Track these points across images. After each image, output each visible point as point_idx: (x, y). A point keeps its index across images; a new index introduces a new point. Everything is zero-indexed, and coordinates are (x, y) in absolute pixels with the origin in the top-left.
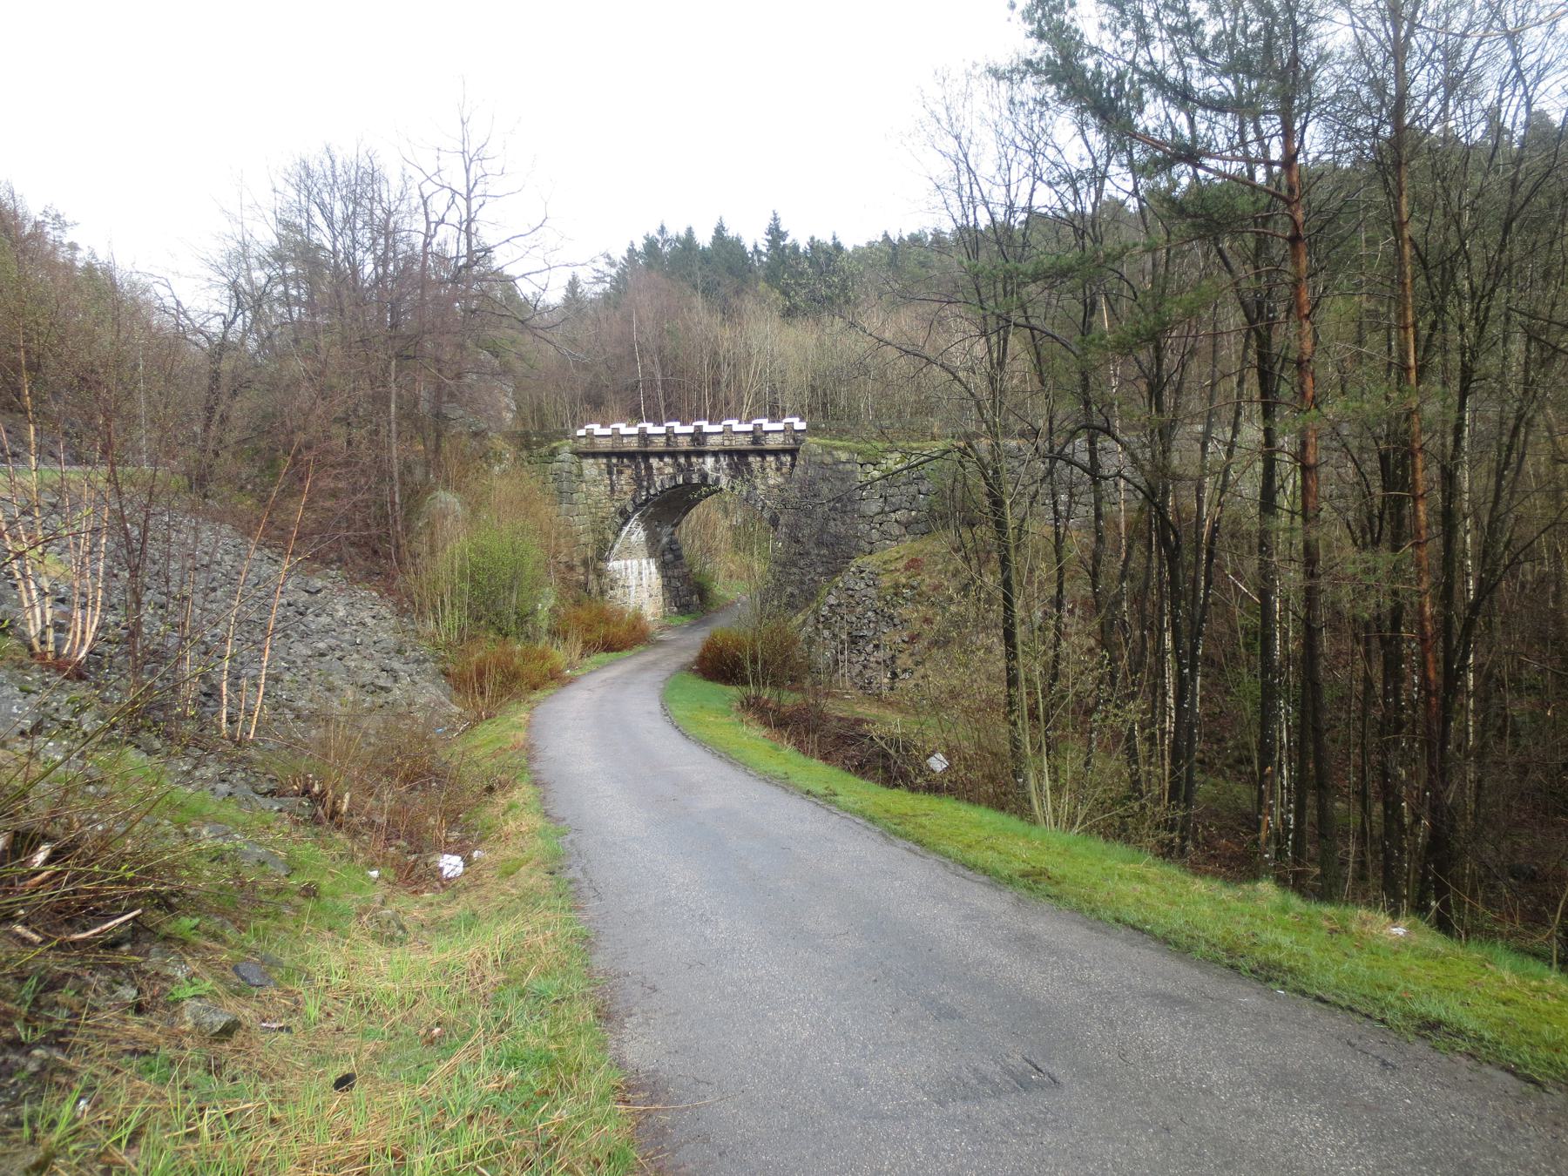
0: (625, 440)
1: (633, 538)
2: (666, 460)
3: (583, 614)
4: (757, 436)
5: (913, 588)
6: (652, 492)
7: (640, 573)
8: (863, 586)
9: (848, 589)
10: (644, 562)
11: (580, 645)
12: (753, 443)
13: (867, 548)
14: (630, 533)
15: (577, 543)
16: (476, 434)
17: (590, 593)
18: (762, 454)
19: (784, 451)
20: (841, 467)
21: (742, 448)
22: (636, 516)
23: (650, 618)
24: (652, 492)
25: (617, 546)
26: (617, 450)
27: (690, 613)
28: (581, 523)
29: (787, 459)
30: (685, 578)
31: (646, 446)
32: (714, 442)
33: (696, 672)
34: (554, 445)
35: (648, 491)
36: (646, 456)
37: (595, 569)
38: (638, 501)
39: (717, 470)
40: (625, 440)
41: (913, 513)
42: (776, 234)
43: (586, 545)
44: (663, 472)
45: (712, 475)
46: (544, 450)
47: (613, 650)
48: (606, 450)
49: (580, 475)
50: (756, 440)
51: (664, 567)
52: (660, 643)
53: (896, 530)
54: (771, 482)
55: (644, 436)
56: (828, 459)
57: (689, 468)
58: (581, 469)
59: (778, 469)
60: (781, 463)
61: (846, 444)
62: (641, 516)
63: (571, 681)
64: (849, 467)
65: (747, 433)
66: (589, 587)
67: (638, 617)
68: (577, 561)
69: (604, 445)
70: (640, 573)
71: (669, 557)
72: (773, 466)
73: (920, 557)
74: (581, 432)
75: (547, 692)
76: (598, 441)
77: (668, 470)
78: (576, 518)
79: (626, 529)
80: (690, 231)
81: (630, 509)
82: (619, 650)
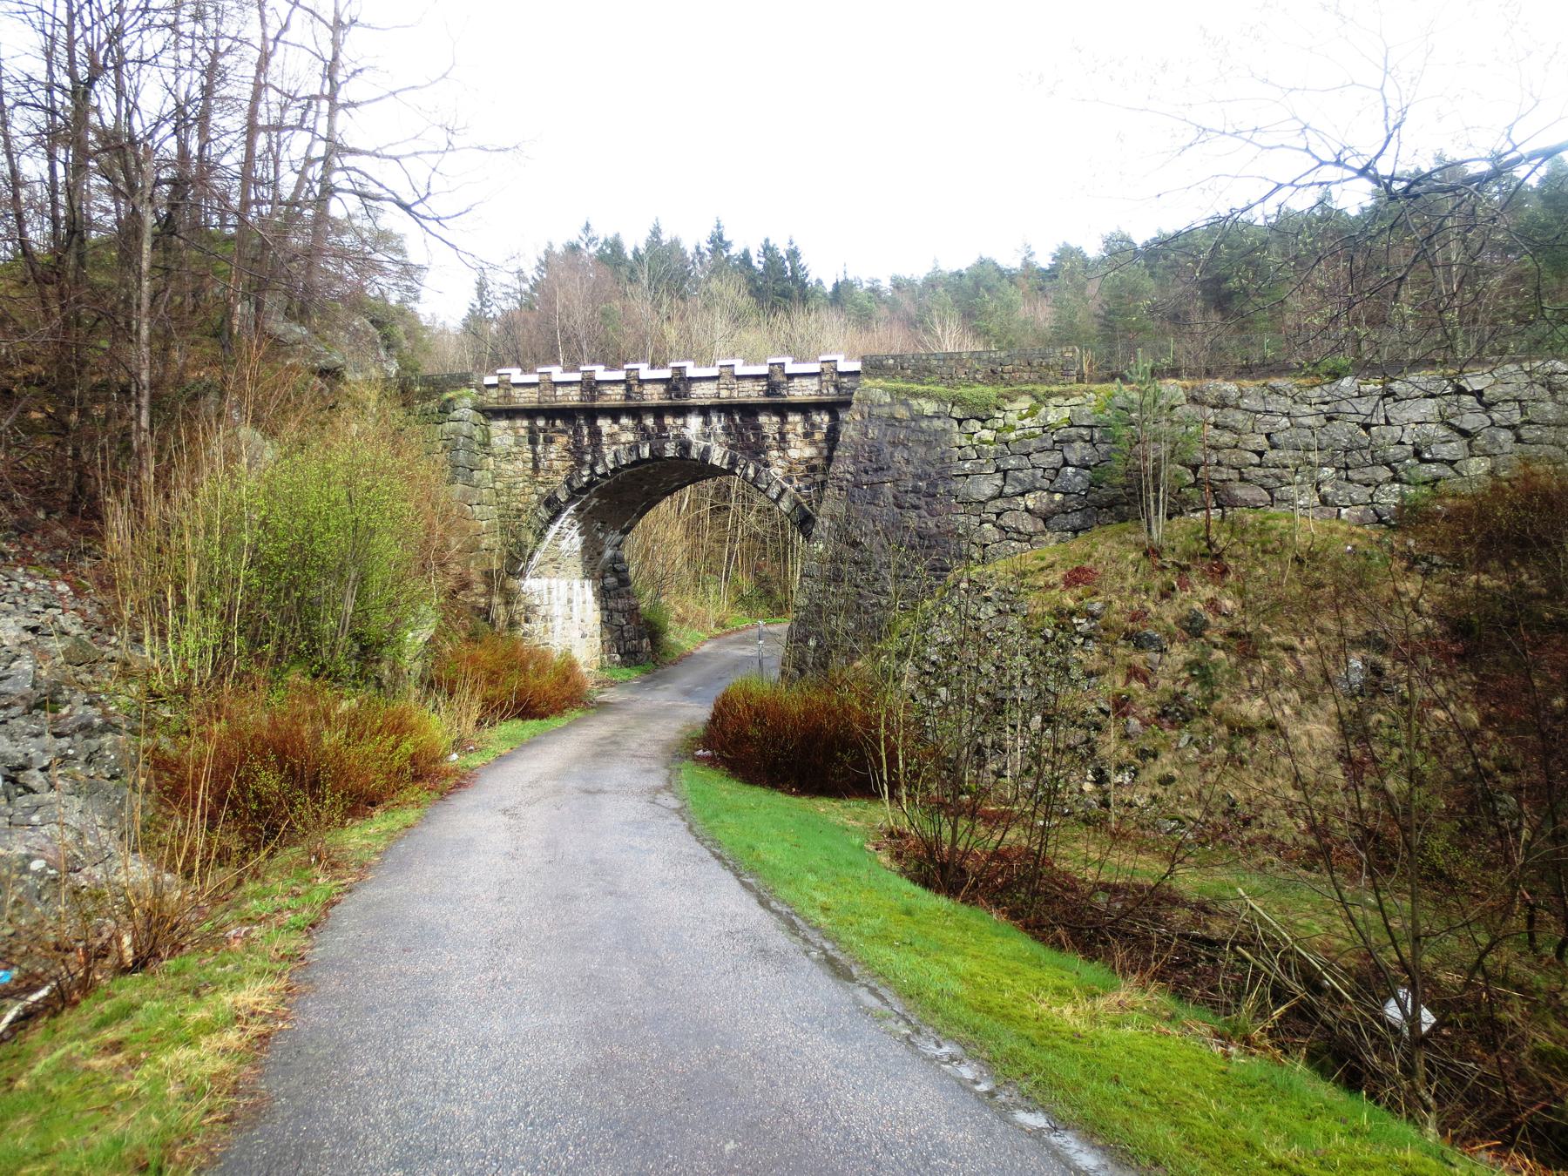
1: (564, 545)
3: (483, 654)
5: (1092, 616)
6: (599, 470)
7: (570, 601)
10: (577, 584)
12: (767, 394)
14: (559, 536)
15: (474, 548)
16: (323, 373)
17: (493, 624)
18: (781, 410)
19: (819, 406)
20: (924, 424)
21: (750, 400)
22: (571, 509)
23: (585, 670)
25: (538, 556)
26: (545, 405)
27: (637, 664)
28: (485, 517)
29: (823, 419)
30: (633, 612)
31: (593, 399)
32: (702, 393)
33: (712, 762)
34: (448, 395)
35: (592, 467)
36: (592, 414)
37: (502, 588)
38: (576, 485)
39: (707, 437)
40: (560, 391)
41: (1058, 497)
42: (718, 243)
43: (490, 550)
46: (432, 405)
48: (529, 405)
49: (486, 444)
50: (773, 389)
51: (604, 594)
52: (603, 707)
53: (1028, 524)
54: (794, 453)
55: (591, 386)
56: (901, 412)
58: (488, 435)
59: (807, 435)
60: (813, 425)
61: (932, 388)
62: (579, 510)
63: (462, 781)
64: (938, 424)
65: (757, 377)
66: (493, 615)
67: (572, 665)
68: (475, 575)
69: (525, 398)
70: (570, 601)
71: (611, 580)
72: (800, 430)
73: (1088, 564)
78: (477, 509)
79: (554, 528)
82: (542, 716)
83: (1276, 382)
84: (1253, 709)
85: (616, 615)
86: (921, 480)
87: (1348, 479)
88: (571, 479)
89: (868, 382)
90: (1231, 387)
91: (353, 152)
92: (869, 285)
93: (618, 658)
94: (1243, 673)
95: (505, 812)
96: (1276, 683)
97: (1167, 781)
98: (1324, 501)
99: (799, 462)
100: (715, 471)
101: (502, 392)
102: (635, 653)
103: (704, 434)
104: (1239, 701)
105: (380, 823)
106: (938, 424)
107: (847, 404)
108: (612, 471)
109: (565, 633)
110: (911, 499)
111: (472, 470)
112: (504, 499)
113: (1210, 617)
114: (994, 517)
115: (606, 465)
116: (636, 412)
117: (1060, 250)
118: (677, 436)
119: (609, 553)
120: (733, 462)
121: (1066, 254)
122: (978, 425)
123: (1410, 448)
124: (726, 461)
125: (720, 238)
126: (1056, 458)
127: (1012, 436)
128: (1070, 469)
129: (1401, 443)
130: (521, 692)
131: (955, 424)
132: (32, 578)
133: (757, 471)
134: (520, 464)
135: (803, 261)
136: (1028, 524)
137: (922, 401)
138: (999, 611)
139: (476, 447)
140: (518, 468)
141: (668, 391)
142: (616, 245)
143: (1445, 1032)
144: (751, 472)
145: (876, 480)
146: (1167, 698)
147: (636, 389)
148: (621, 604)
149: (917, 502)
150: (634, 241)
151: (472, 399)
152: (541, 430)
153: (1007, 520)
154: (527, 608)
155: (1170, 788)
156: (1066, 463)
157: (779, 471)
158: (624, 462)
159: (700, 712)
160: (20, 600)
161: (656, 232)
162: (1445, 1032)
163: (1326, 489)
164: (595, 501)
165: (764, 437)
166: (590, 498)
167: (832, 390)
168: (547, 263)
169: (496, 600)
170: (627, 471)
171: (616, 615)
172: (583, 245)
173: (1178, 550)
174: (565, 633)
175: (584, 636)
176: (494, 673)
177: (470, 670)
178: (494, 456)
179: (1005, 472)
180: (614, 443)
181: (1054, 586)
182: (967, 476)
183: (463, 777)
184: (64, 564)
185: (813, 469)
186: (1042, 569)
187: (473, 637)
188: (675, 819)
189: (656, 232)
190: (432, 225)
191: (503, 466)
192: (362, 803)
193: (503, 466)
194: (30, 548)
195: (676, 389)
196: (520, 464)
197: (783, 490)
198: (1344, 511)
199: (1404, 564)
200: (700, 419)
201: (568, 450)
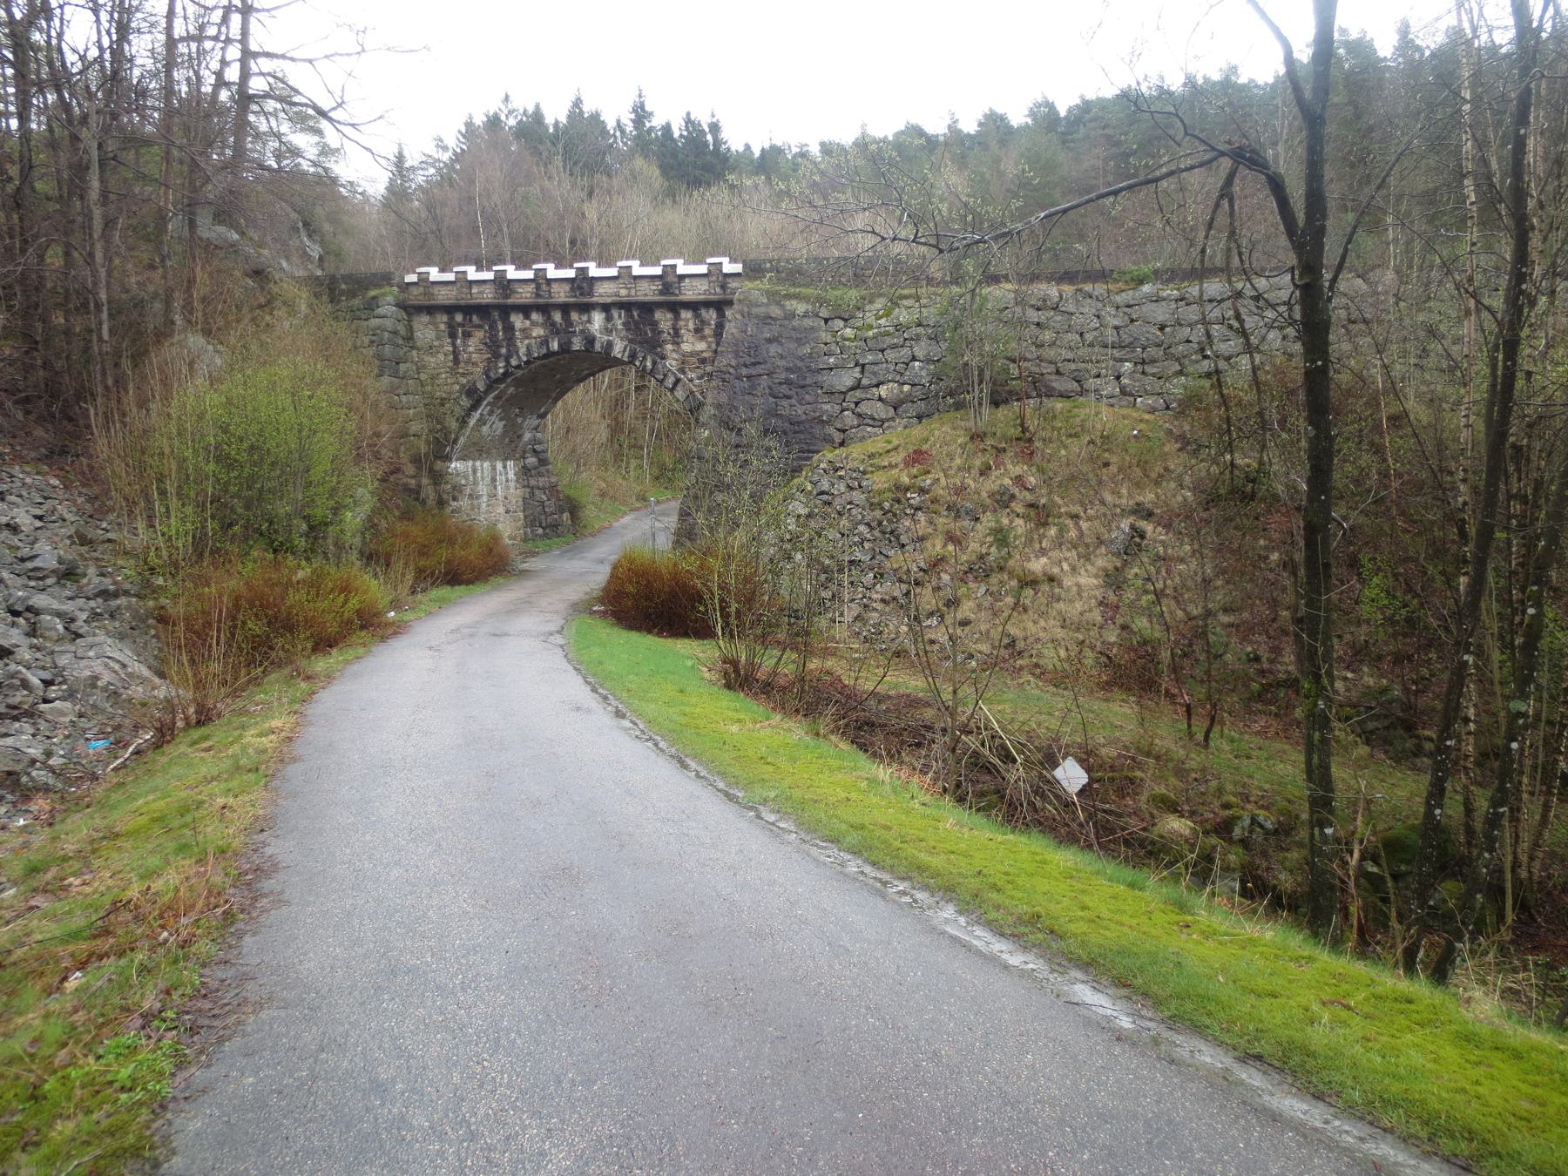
0: (475, 290)
1: (485, 429)
2: (535, 316)
3: (414, 530)
4: (669, 281)
5: (922, 491)
6: (514, 362)
7: (494, 480)
8: (843, 489)
9: (822, 493)
11: (410, 577)
12: (661, 293)
13: (838, 437)
17: (424, 502)
18: (675, 307)
19: (707, 304)
21: (647, 299)
22: (490, 398)
23: (508, 541)
24: (514, 362)
25: (462, 440)
26: (462, 302)
29: (711, 315)
30: (553, 489)
31: (507, 297)
32: (603, 292)
33: (603, 614)
34: (372, 293)
36: (506, 310)
37: (431, 470)
41: (906, 388)
42: (641, 114)
44: (530, 335)
45: (601, 339)
46: (356, 302)
47: (460, 583)
49: (409, 338)
54: (686, 347)
55: (502, 283)
56: (775, 311)
57: (565, 331)
58: (411, 329)
59: (697, 330)
60: (703, 322)
61: (804, 290)
62: (498, 398)
63: (398, 629)
66: (423, 495)
67: (495, 538)
69: (444, 296)
71: (531, 460)
72: (691, 326)
73: (925, 447)
74: (411, 278)
75: (350, 654)
76: (436, 290)
77: (538, 332)
78: (404, 399)
79: (476, 415)
80: (537, 106)
81: (481, 386)
82: (469, 582)
83: (1088, 287)
84: (1037, 565)
85: (537, 492)
86: (793, 373)
87: (1143, 373)
88: (489, 370)
89: (749, 285)
90: (1053, 291)
91: (268, 55)
92: (798, 150)
93: (540, 531)
94: (1036, 537)
95: (430, 648)
96: (1060, 545)
97: (965, 623)
98: (1123, 392)
99: (692, 354)
100: (617, 362)
101: (421, 289)
102: (556, 526)
103: (606, 329)
104: (1029, 560)
105: (336, 657)
106: (808, 322)
107: (730, 303)
108: (525, 363)
109: (490, 509)
110: (784, 389)
111: (398, 363)
112: (429, 388)
113: (1016, 491)
114: (853, 406)
115: (519, 357)
116: (545, 309)
117: (985, 116)
118: (582, 331)
119: (527, 436)
120: (633, 356)
121: (995, 123)
122: (841, 323)
123: (1196, 346)
124: (627, 354)
125: (642, 106)
126: (905, 352)
127: (870, 333)
128: (917, 363)
129: (1188, 341)
130: (448, 562)
131: (823, 323)
132: (28, 473)
133: (654, 363)
134: (441, 357)
135: (724, 135)
136: (881, 411)
137: (794, 302)
138: (848, 486)
139: (400, 342)
140: (441, 359)
141: (572, 289)
142: (537, 116)
143: (1096, 786)
144: (649, 364)
145: (754, 373)
146: (974, 557)
147: (544, 287)
148: (542, 481)
149: (790, 393)
150: (556, 114)
151: (395, 296)
152: (459, 325)
153: (864, 408)
154: (454, 488)
155: (967, 629)
156: (914, 359)
157: (674, 363)
158: (536, 355)
159: (599, 577)
160: (24, 493)
161: (577, 103)
162: (1096, 786)
163: (1125, 381)
164: (511, 390)
165: (660, 333)
166: (507, 387)
167: (718, 290)
168: (470, 131)
169: (425, 481)
170: (539, 362)
171: (537, 492)
172: (503, 118)
173: (998, 434)
174: (490, 509)
175: (507, 512)
176: (425, 546)
177: (403, 545)
178: (418, 349)
179: (863, 366)
180: (527, 338)
181: (896, 465)
182: (831, 369)
183: (399, 627)
184: (55, 456)
185: (703, 361)
186: (888, 451)
187: (407, 516)
188: (559, 651)
189: (577, 103)
190: (348, 130)
191: (426, 358)
192: (324, 644)
193: (426, 358)
194: (18, 448)
195: (580, 288)
196: (441, 357)
197: (678, 381)
198: (1139, 400)
199: (1178, 446)
200: (603, 315)
201: (486, 344)
